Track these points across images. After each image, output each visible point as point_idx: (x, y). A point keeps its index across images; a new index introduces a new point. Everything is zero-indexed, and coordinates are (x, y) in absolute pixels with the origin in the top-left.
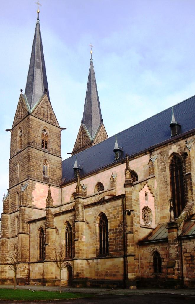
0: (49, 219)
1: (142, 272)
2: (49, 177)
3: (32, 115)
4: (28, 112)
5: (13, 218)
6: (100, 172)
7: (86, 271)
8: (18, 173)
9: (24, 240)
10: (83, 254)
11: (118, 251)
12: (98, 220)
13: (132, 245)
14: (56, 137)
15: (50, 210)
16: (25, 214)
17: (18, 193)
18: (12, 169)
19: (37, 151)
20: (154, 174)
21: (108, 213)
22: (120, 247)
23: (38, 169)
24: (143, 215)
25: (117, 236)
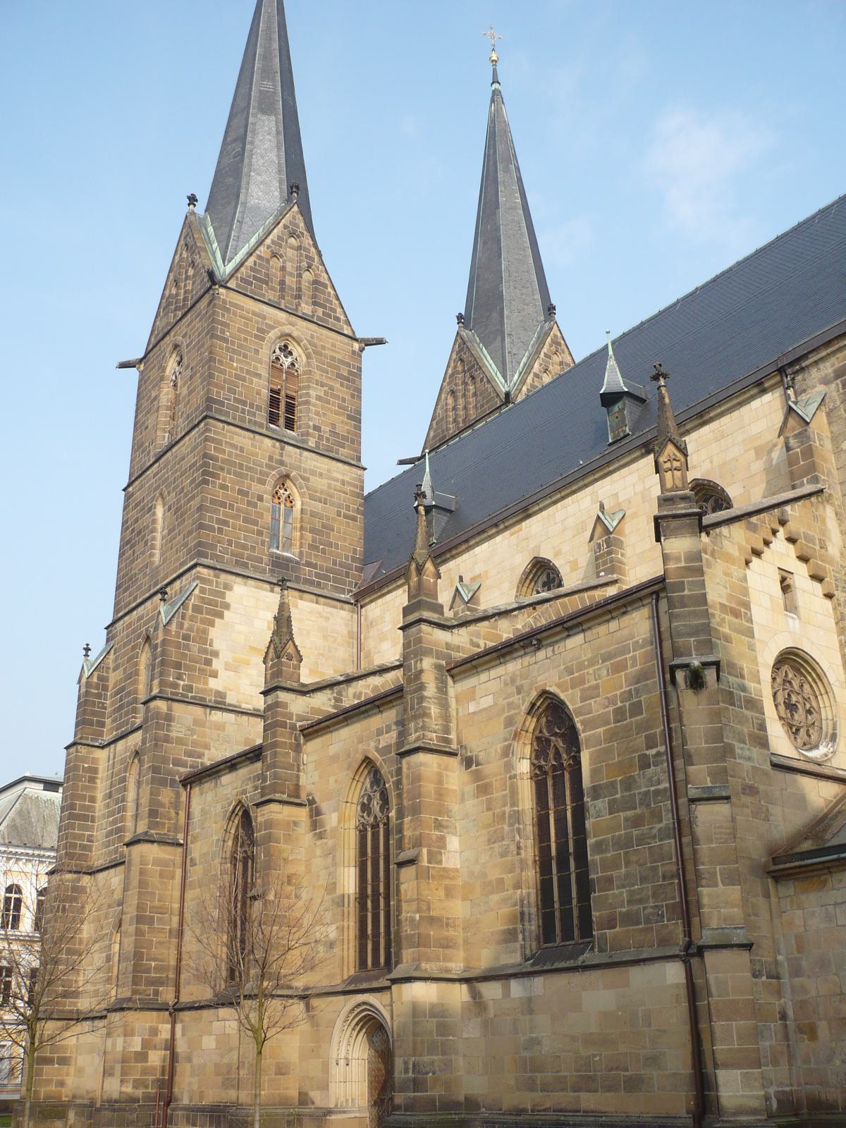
0: (275, 755)
1: (807, 1060)
2: (301, 553)
3: (229, 285)
4: (211, 274)
5: (117, 768)
6: (541, 510)
7: (465, 1056)
8: (158, 543)
9: (154, 880)
10: (447, 944)
11: (648, 921)
12: (528, 738)
13: (730, 879)
14: (339, 376)
15: (285, 705)
16: (167, 739)
17: (148, 639)
18: (133, 531)
19: (243, 439)
20: (815, 480)
21: (577, 692)
22: (655, 895)
23: (246, 520)
24: (780, 699)
25: (637, 822)
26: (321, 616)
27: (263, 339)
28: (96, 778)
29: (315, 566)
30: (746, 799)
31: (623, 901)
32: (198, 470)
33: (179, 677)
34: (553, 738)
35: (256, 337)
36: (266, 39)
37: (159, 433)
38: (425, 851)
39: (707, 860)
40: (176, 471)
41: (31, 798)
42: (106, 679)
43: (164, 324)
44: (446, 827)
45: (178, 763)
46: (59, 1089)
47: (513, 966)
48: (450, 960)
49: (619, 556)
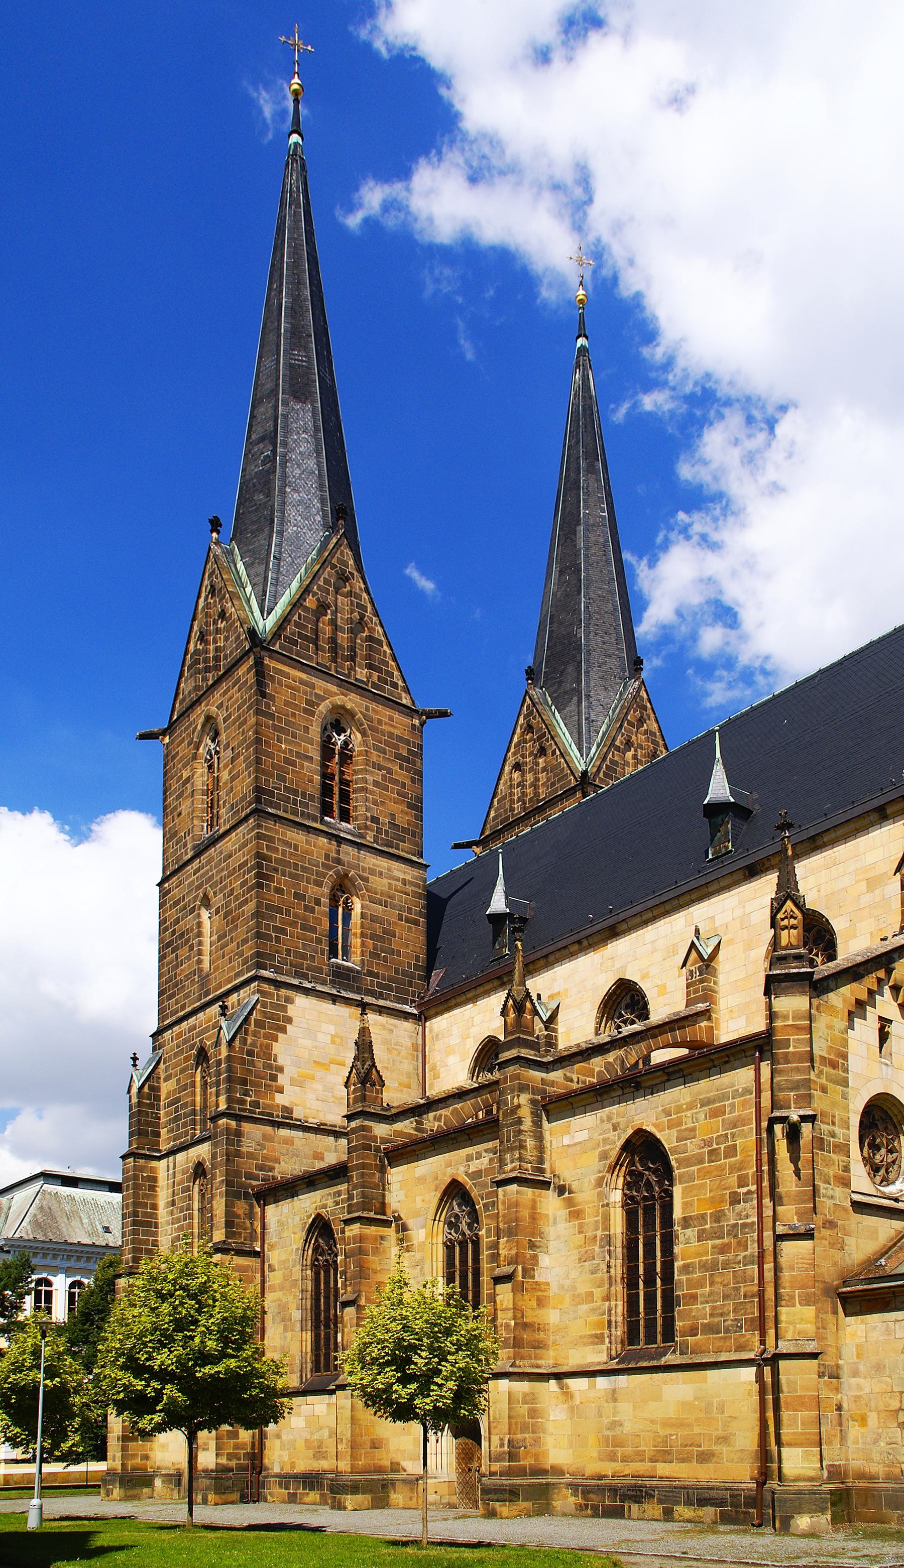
2: (363, 961)
8: (206, 948)
11: (727, 1330)
13: (807, 1301)
14: (398, 756)
16: (238, 1154)
18: (174, 932)
19: (297, 837)
21: (674, 1133)
22: (735, 1311)
26: (384, 1029)
27: (312, 714)
28: (156, 1186)
29: (376, 976)
30: (825, 1232)
31: (706, 1314)
32: (249, 871)
33: (246, 1093)
34: (647, 1173)
35: (305, 711)
36: (293, 283)
37: (196, 822)
38: (520, 1268)
39: (787, 1285)
40: (222, 870)
41: (50, 1194)
42: (158, 1089)
43: (190, 688)
44: (539, 1247)
45: (250, 1176)
46: (144, 1462)
47: (599, 1363)
48: (541, 1358)
49: (712, 984)
